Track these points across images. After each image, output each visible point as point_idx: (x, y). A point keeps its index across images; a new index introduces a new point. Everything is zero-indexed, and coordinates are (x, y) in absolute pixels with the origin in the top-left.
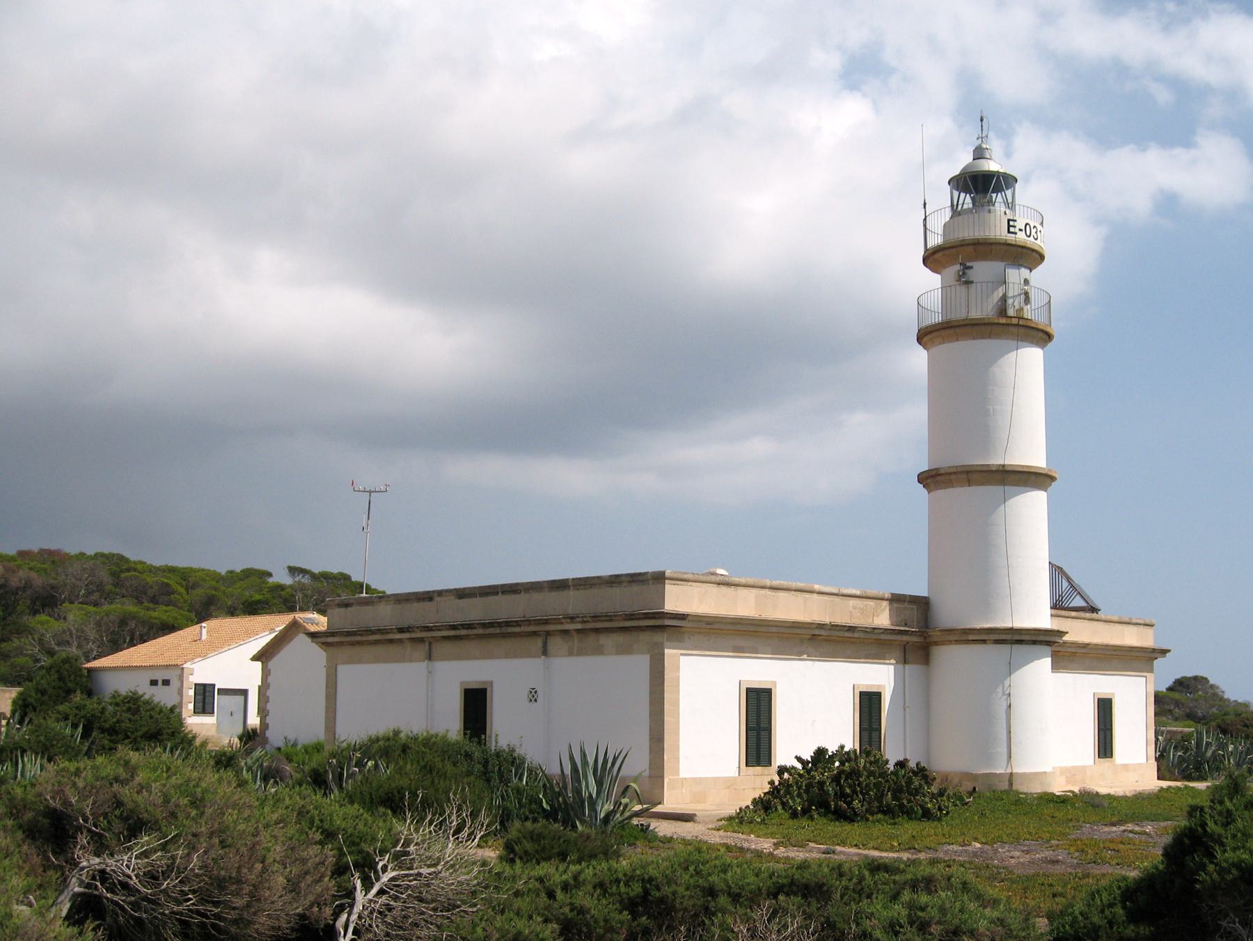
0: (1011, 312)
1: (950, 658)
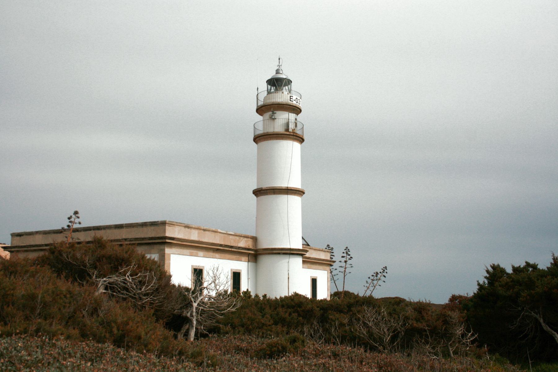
0: (290, 130)
1: (266, 261)
